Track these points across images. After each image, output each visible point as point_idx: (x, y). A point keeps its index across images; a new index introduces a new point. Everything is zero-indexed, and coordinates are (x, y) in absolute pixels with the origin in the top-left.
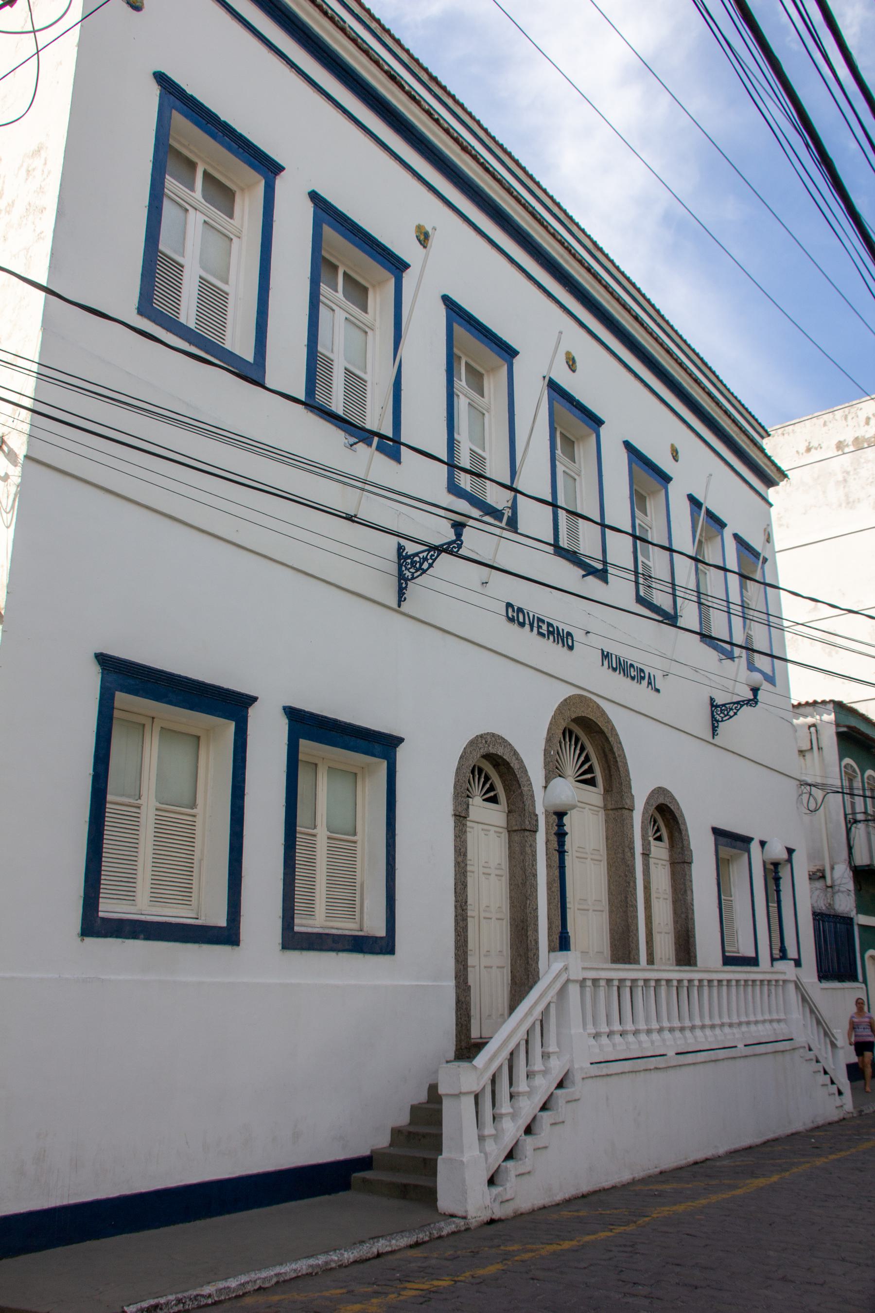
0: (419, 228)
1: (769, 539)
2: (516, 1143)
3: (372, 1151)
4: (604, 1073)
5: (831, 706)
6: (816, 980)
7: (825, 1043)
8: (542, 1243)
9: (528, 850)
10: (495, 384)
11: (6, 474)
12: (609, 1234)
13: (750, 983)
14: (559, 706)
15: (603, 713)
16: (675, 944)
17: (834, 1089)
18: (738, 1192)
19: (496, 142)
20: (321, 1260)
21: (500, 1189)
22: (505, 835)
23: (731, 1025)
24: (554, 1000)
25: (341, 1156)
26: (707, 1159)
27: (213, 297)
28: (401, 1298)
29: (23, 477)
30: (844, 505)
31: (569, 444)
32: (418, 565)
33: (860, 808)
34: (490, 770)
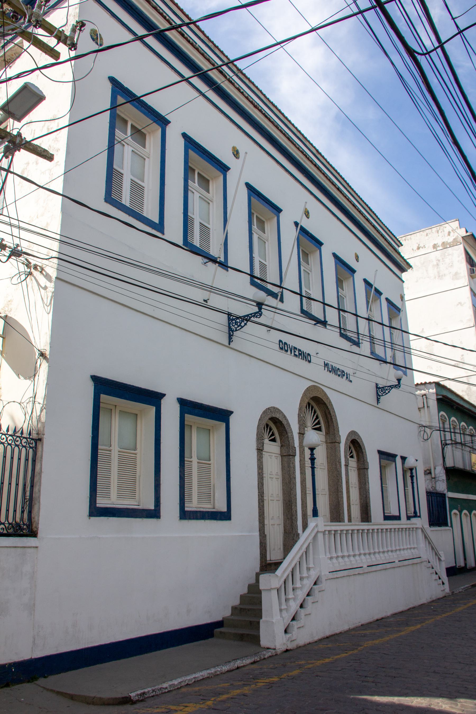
0: (234, 148)
1: (402, 298)
2: (296, 613)
3: (223, 618)
4: (335, 577)
5: (434, 385)
6: (428, 526)
7: (436, 559)
8: (315, 660)
9: (291, 465)
10: (270, 227)
11: (45, 286)
12: (346, 655)
13: (400, 530)
14: (305, 391)
15: (325, 394)
16: (361, 510)
17: (440, 582)
18: (402, 633)
19: (270, 101)
20: (213, 670)
21: (290, 635)
22: (279, 458)
23: (392, 551)
24: (312, 541)
25: (209, 621)
26: (382, 618)
27: (137, 189)
28: (257, 686)
29: (55, 288)
30: (437, 277)
31: (306, 255)
32: (239, 324)
33: (448, 437)
34: (273, 425)
